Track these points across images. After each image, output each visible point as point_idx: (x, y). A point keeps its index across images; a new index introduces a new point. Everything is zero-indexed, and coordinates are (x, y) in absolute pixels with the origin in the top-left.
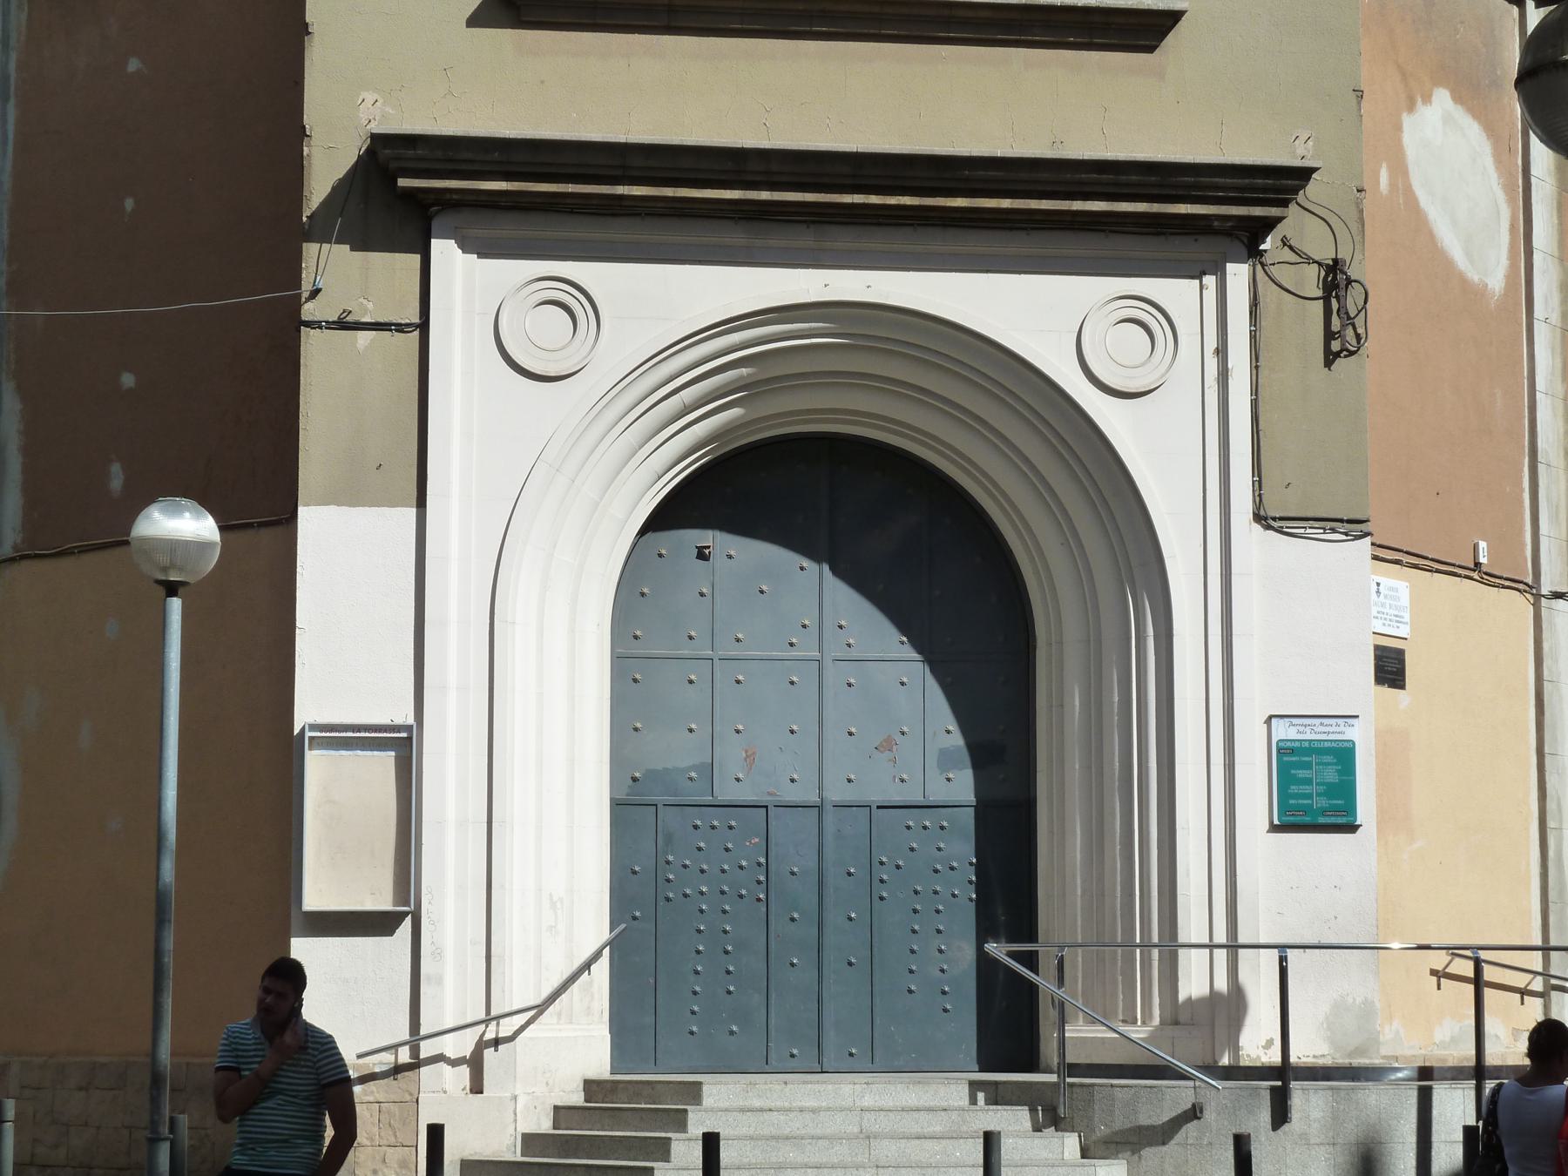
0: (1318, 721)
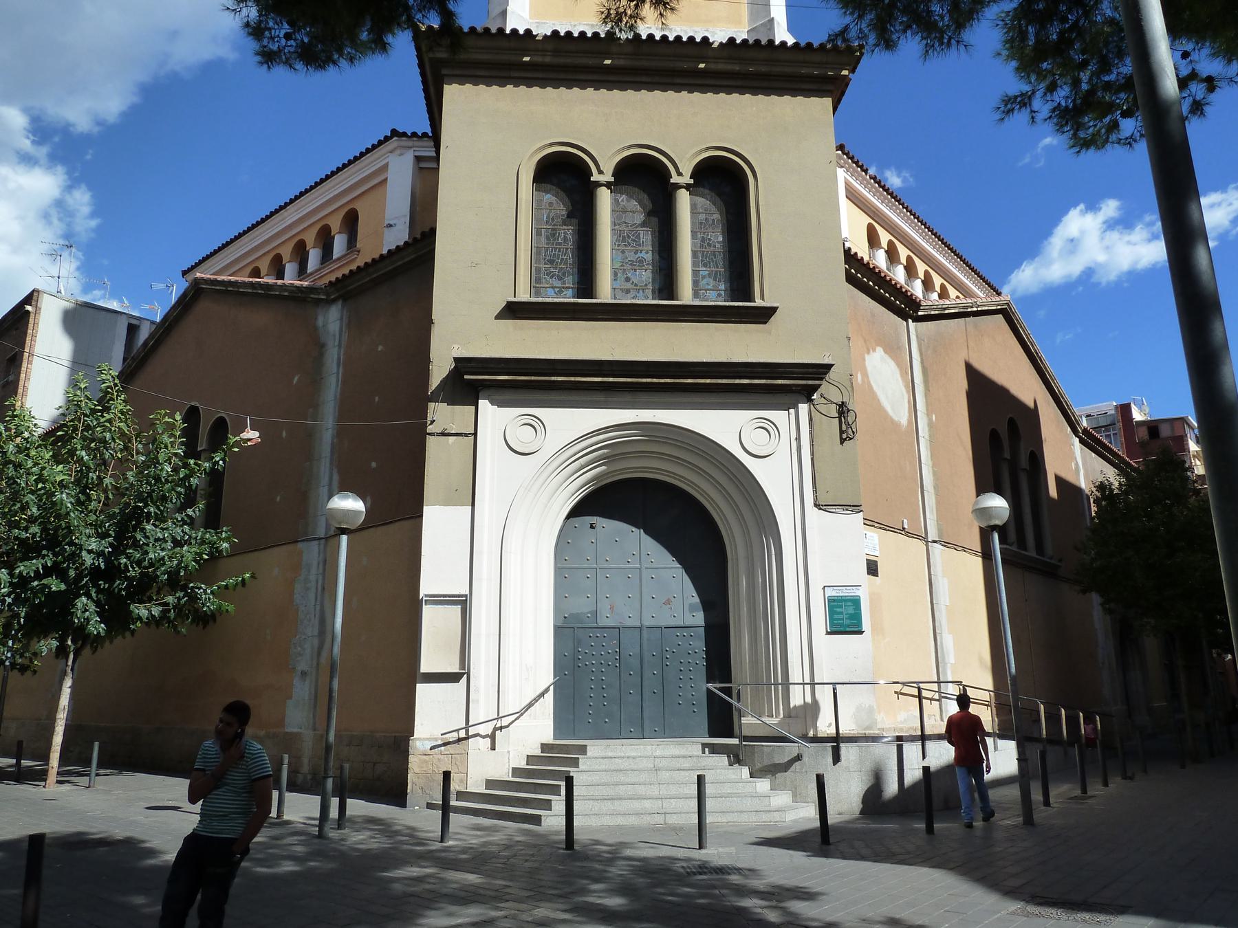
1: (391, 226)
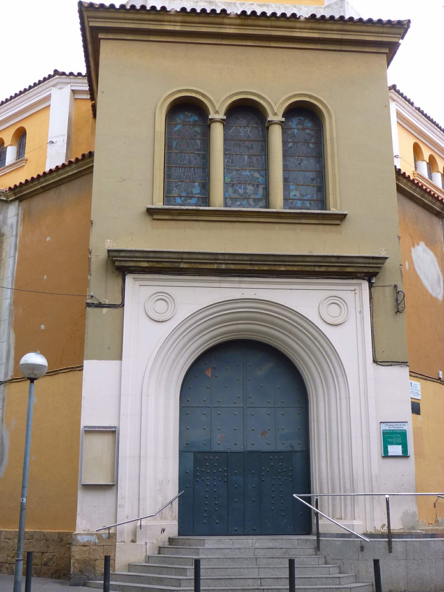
0: (394, 424)
1: (53, 142)
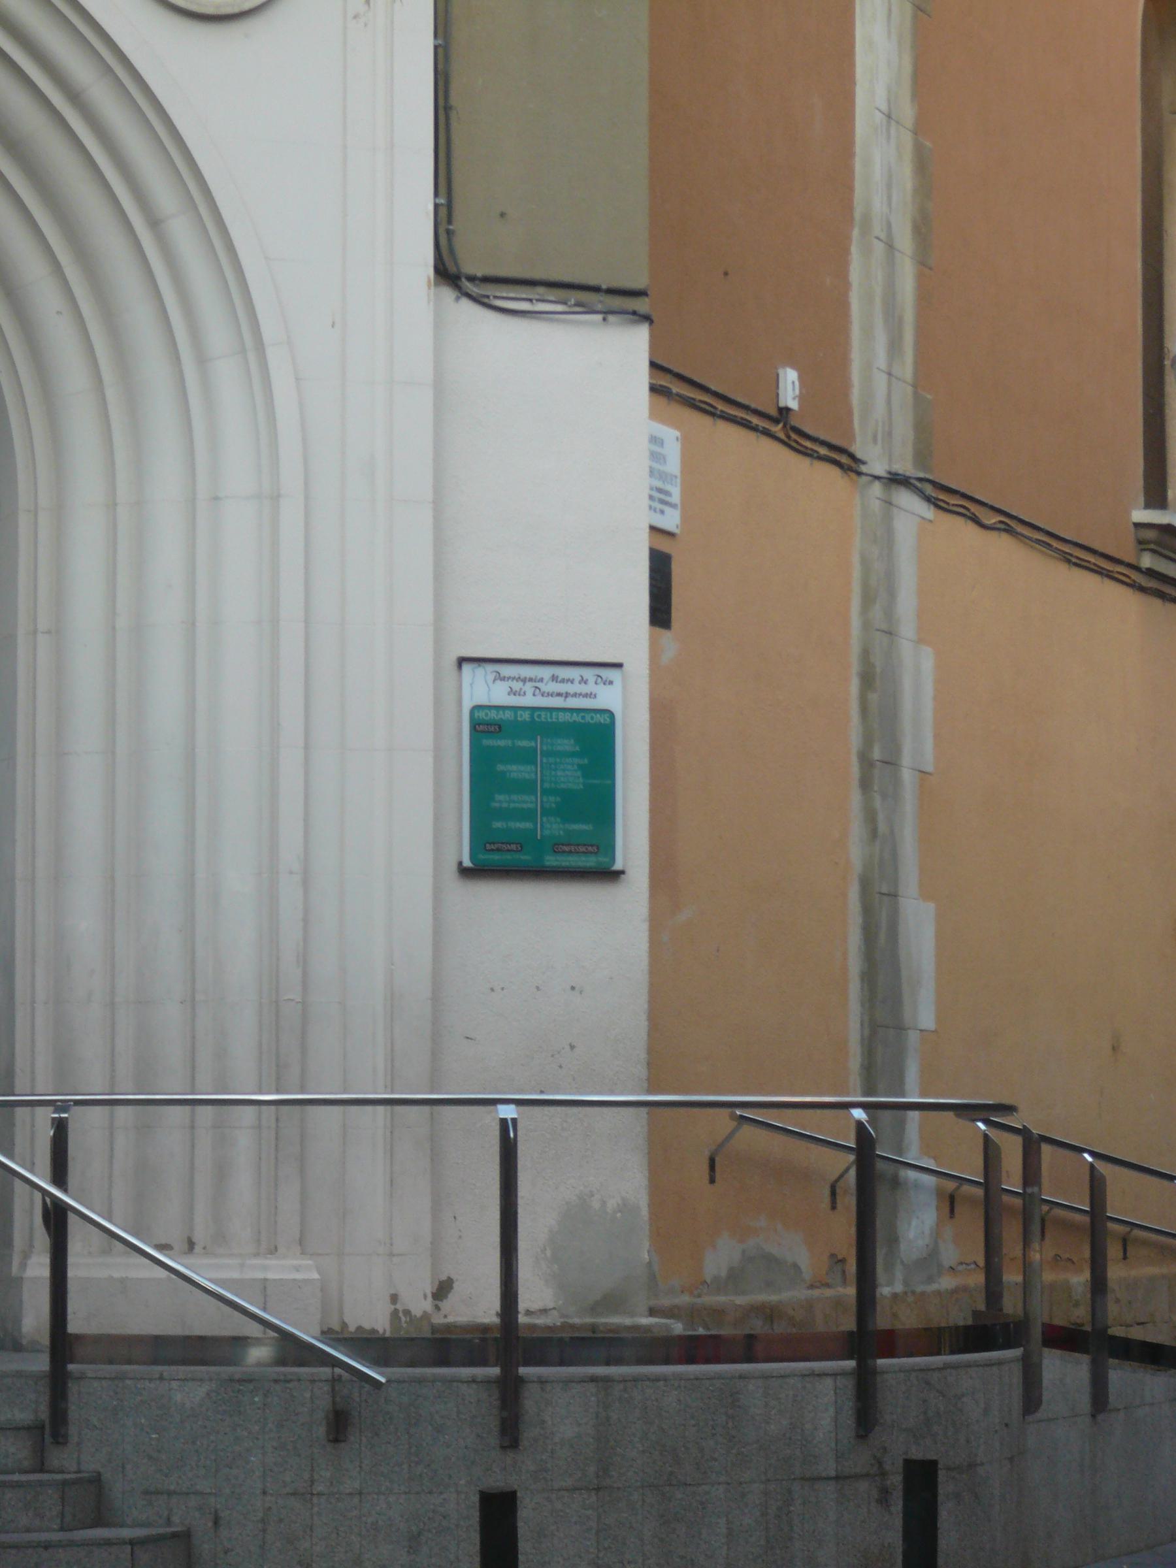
0: (545, 672)
